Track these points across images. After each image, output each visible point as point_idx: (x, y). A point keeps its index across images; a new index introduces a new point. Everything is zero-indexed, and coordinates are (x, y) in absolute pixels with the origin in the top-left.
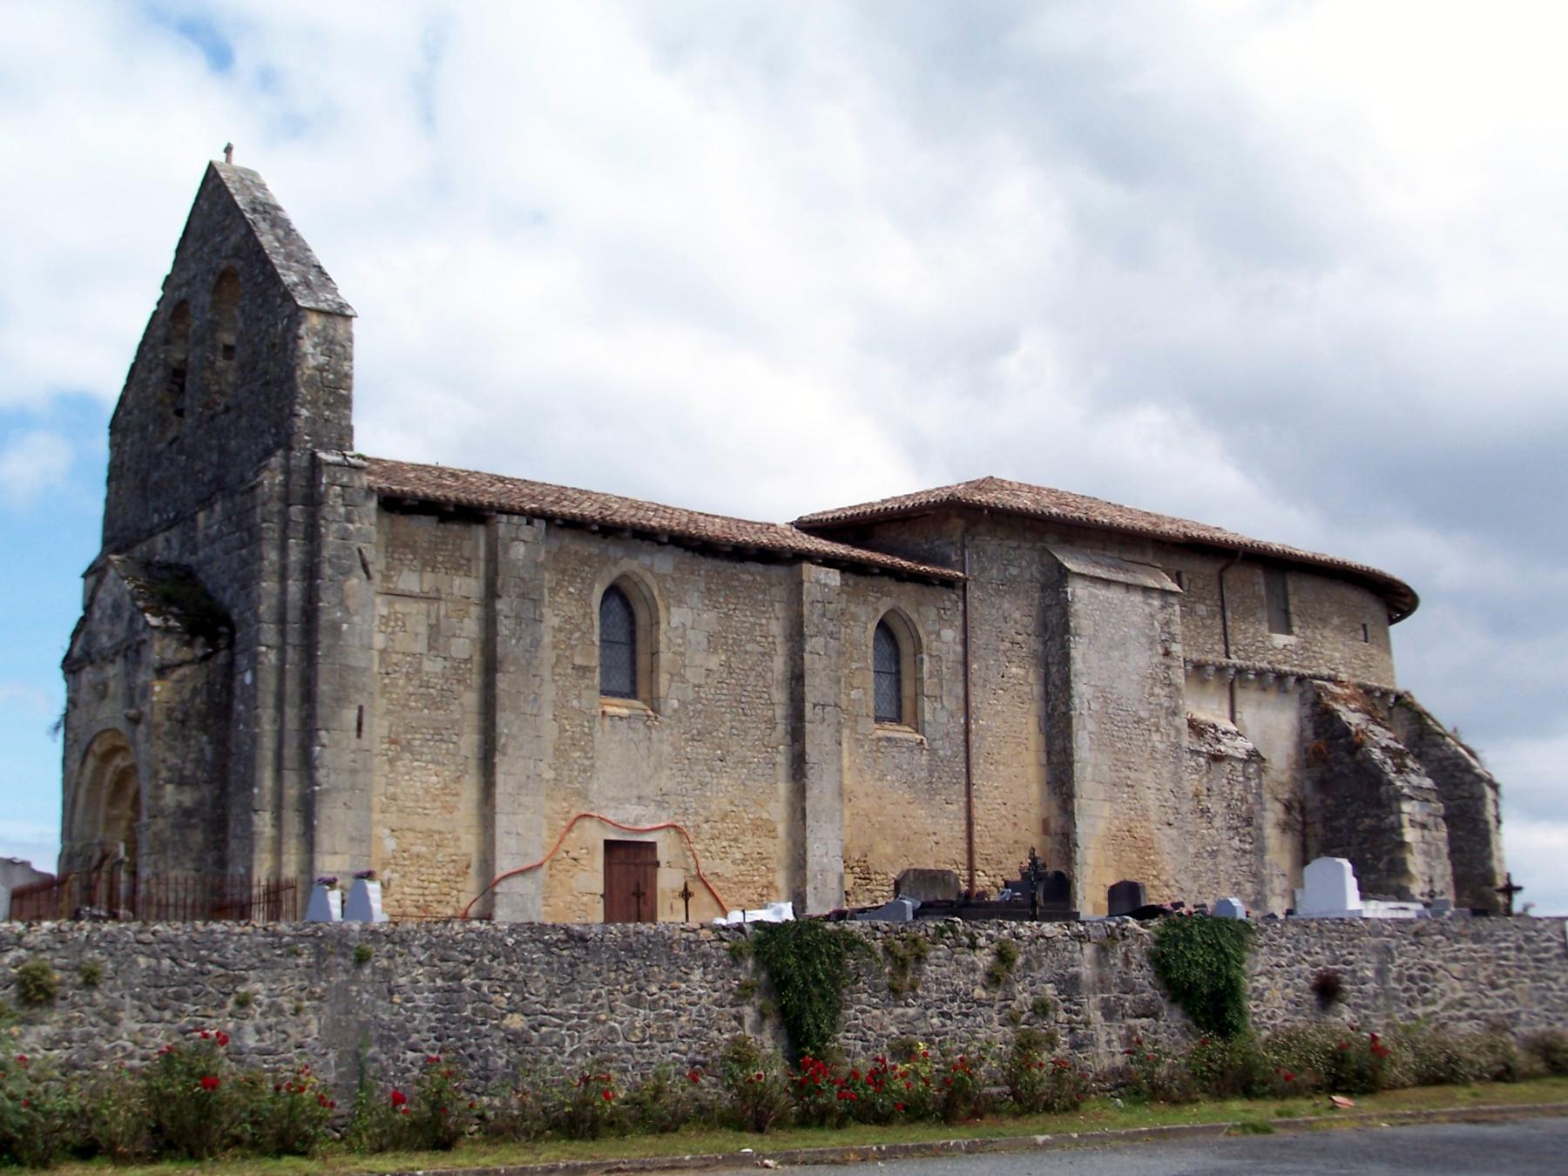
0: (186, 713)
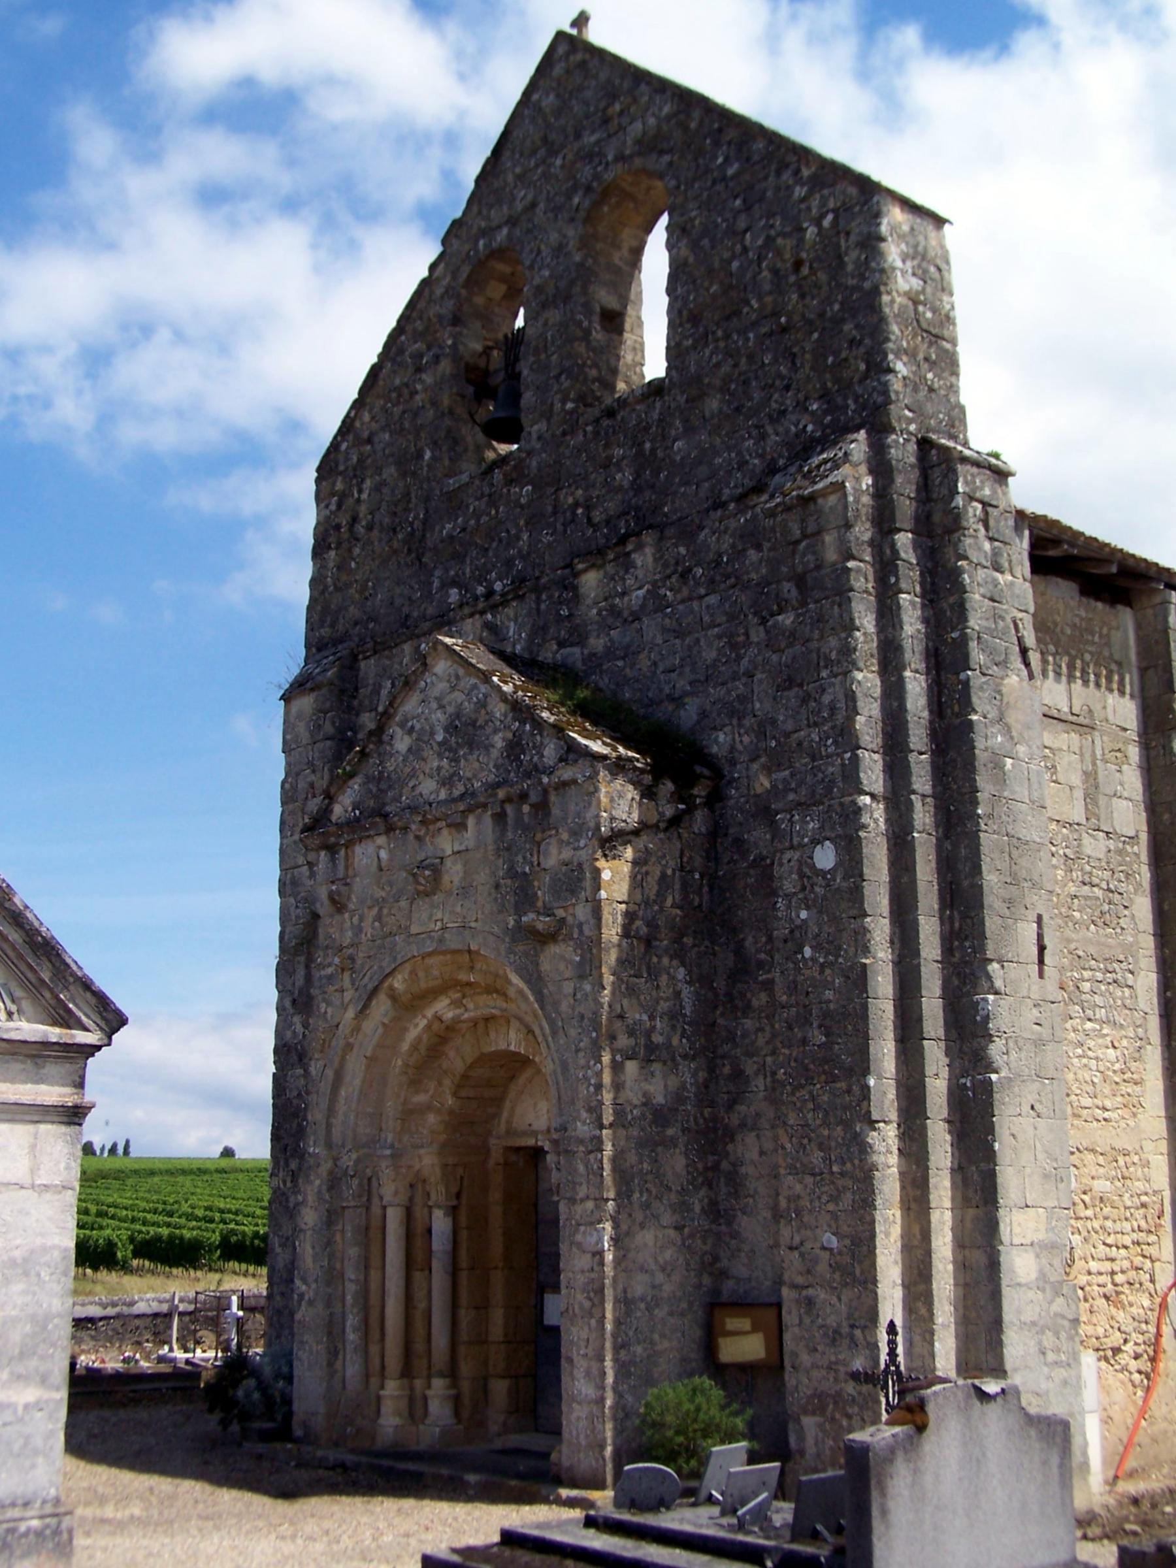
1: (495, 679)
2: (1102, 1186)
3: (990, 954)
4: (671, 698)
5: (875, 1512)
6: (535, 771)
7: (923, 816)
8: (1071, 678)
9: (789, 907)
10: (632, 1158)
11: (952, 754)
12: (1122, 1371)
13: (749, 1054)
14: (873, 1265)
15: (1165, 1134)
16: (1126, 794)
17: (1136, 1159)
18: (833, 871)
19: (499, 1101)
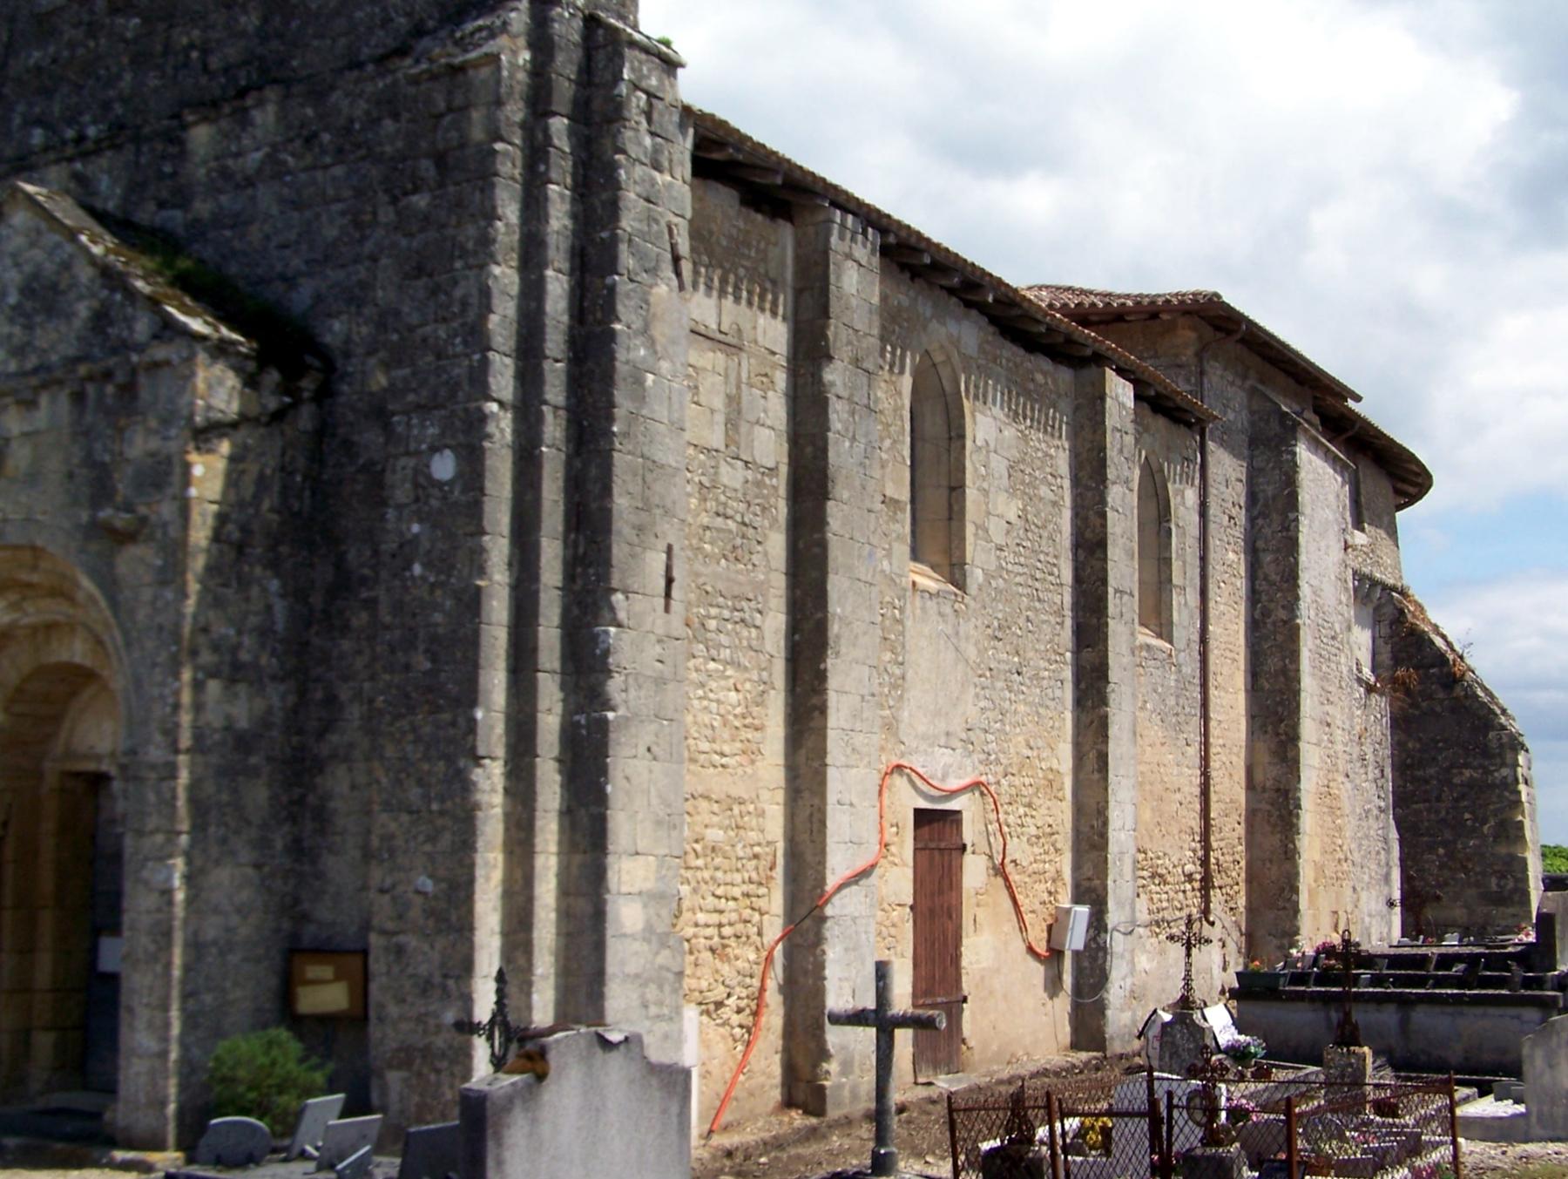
0: (245, 529)
1: (84, 238)
2: (715, 835)
3: (615, 583)
4: (284, 278)
5: (490, 1163)
6: (124, 347)
7: (553, 429)
8: (722, 293)
9: (399, 519)
10: (209, 788)
11: (590, 364)
12: (723, 1025)
13: (346, 679)
14: (470, 912)
15: (782, 783)
16: (769, 422)
17: (751, 808)
18: (450, 483)
19: (56, 719)
